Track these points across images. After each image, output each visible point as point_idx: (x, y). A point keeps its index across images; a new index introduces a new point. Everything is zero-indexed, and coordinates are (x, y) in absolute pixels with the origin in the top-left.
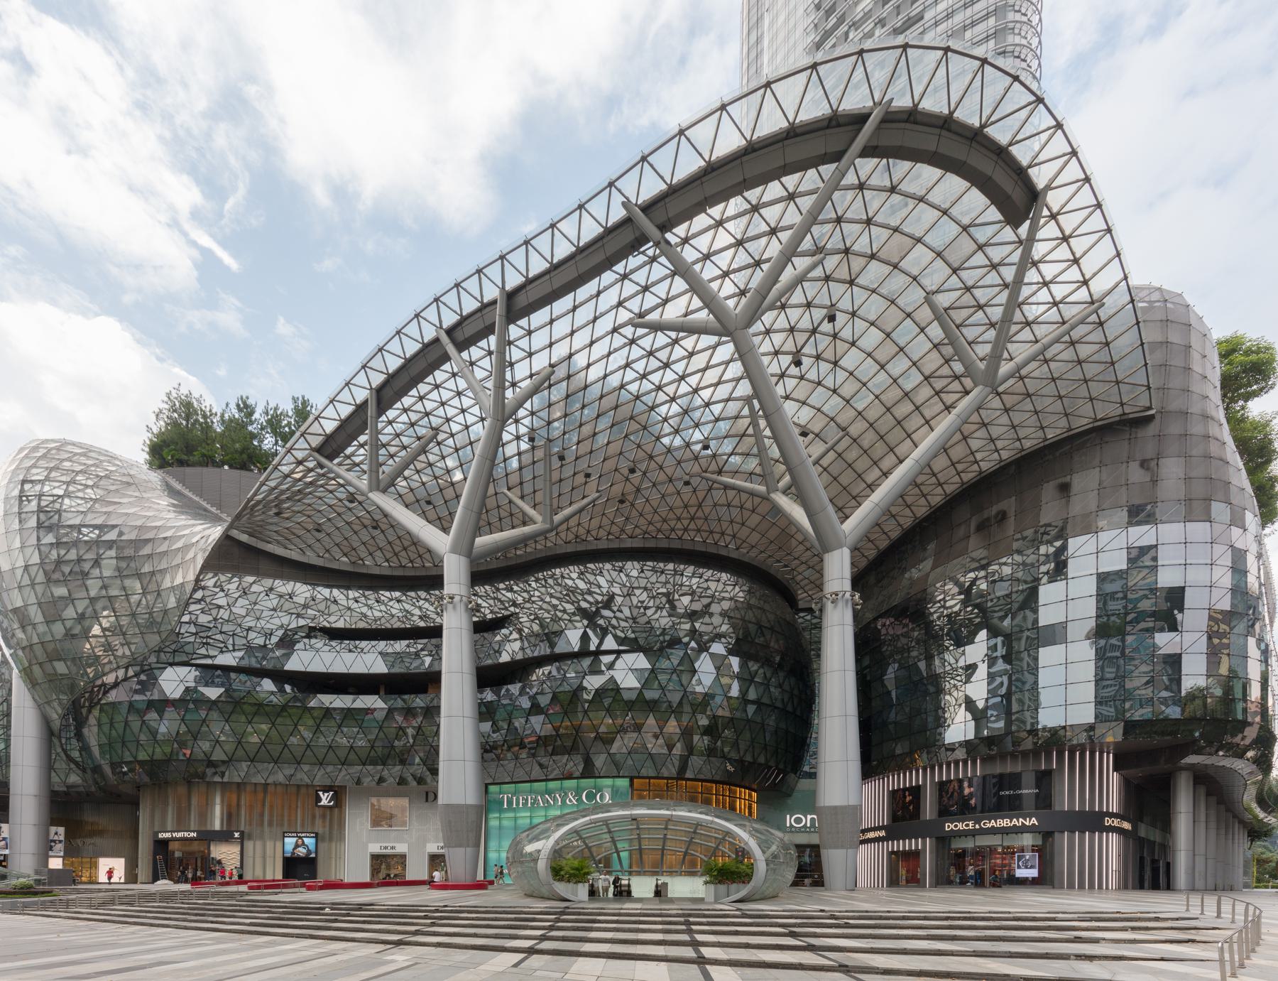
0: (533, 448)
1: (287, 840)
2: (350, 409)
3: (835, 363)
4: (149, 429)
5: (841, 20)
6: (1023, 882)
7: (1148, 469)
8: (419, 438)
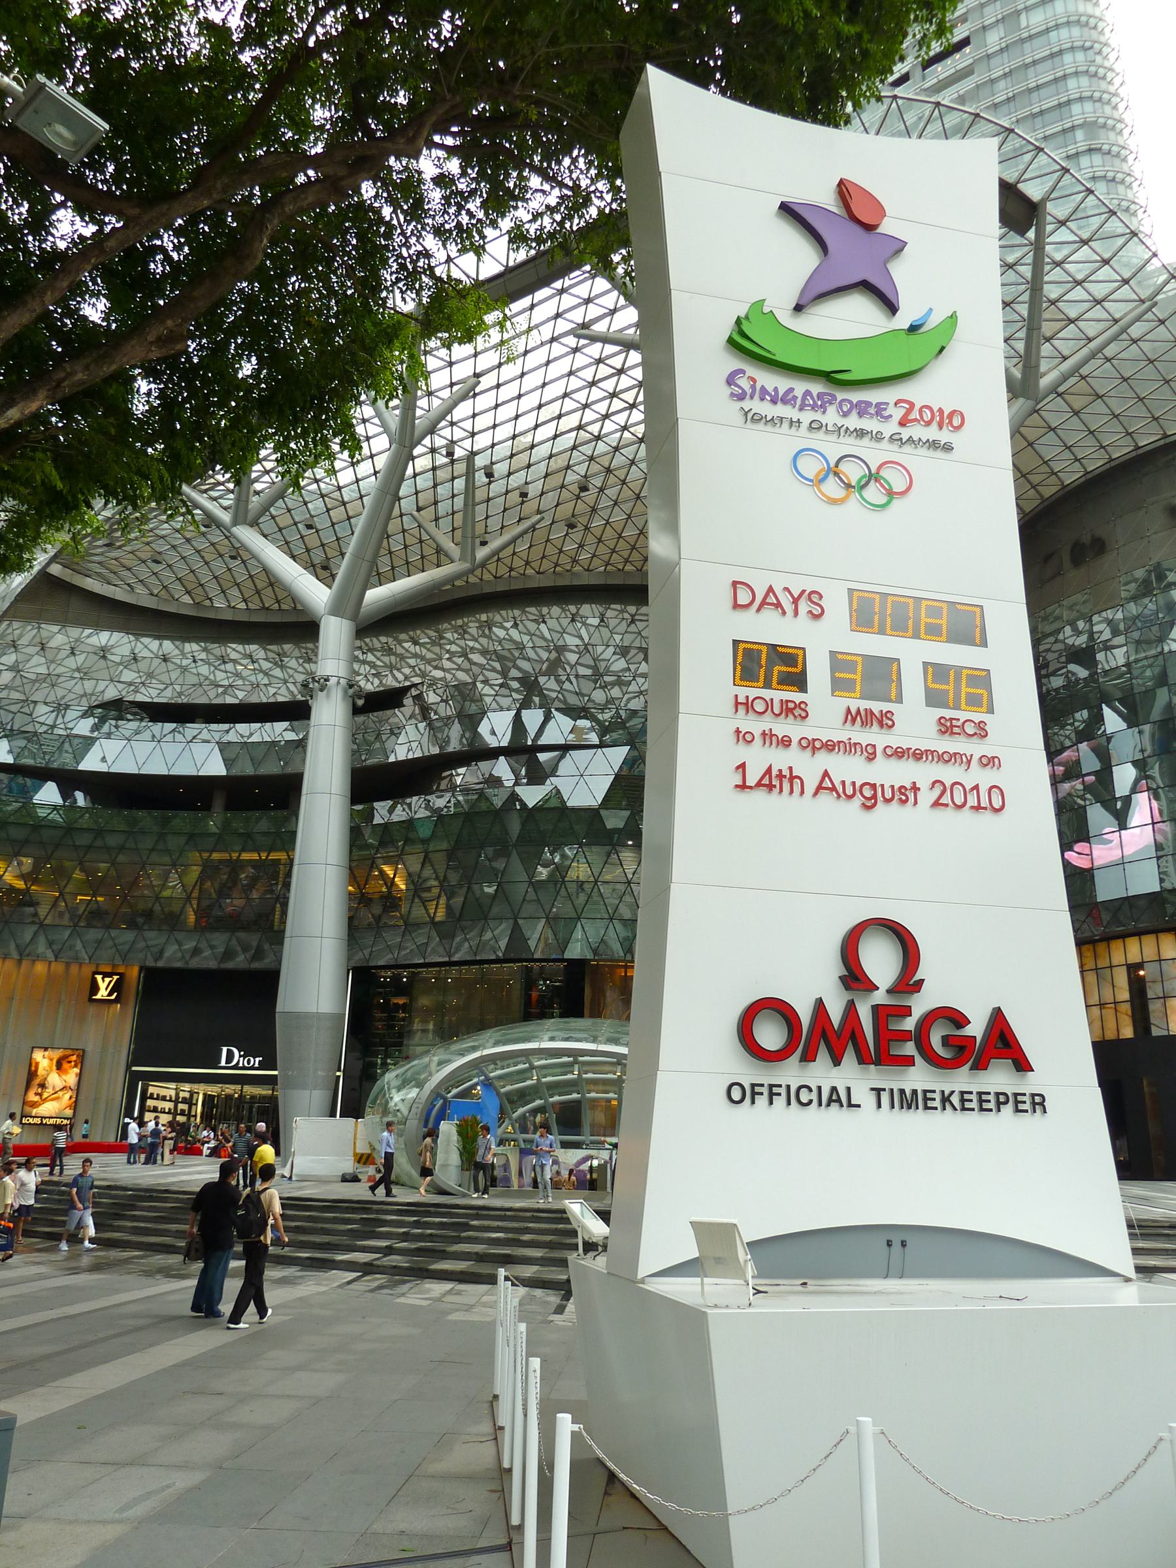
0: (453, 462)
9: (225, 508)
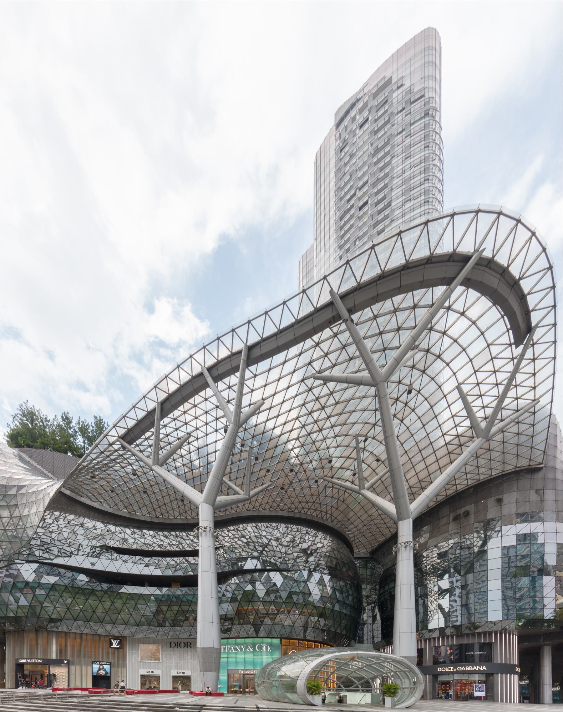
1: (94, 666)
2: (144, 413)
3: (402, 421)
4: (8, 425)
6: (479, 698)
7: (539, 494)
8: (179, 439)
9: (148, 457)
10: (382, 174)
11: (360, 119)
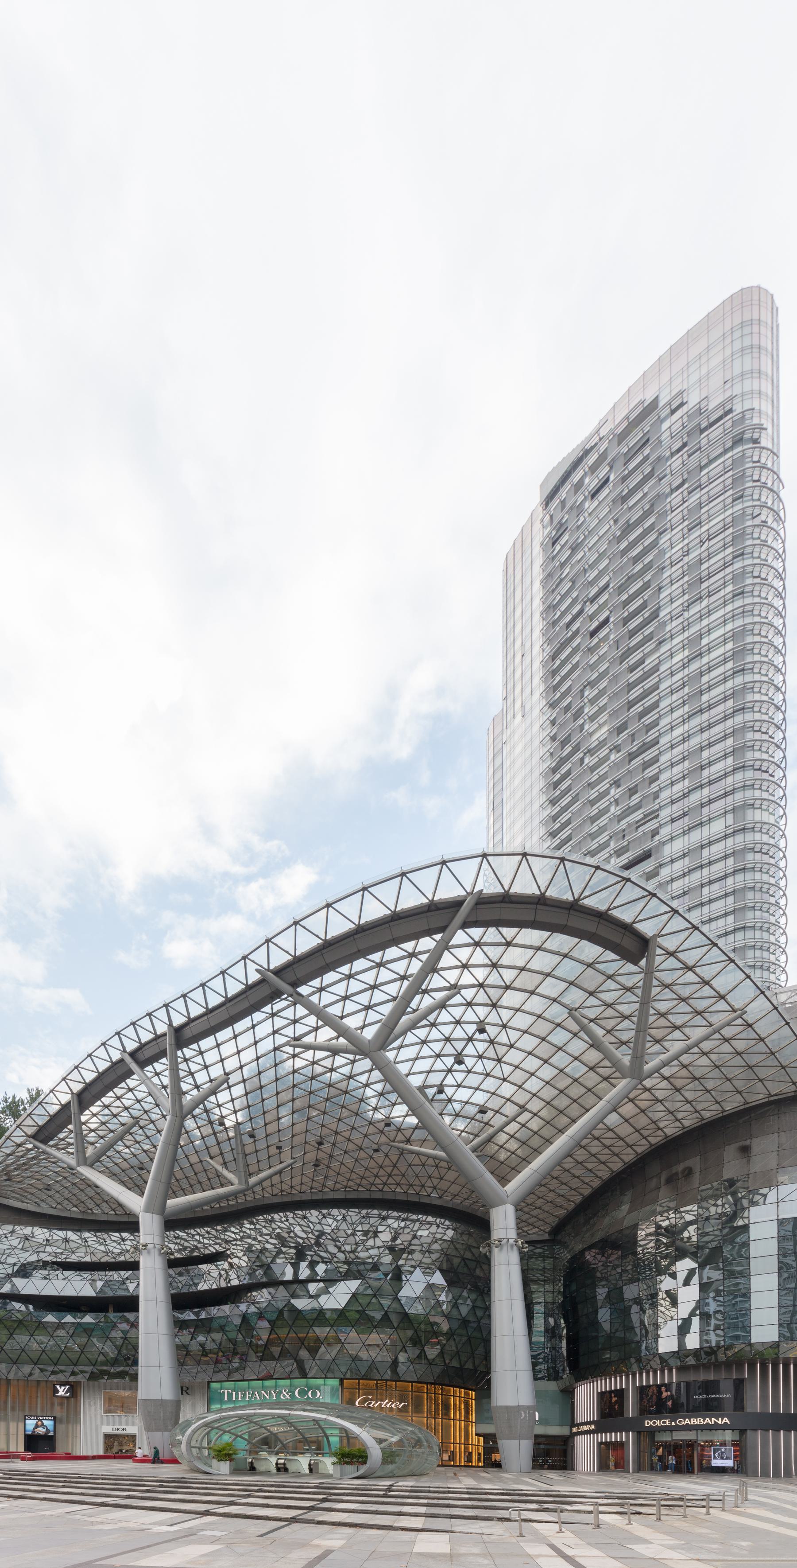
1: (27, 1422)
5: (576, 749)
6: (722, 1470)
10: (639, 566)
11: (591, 483)
